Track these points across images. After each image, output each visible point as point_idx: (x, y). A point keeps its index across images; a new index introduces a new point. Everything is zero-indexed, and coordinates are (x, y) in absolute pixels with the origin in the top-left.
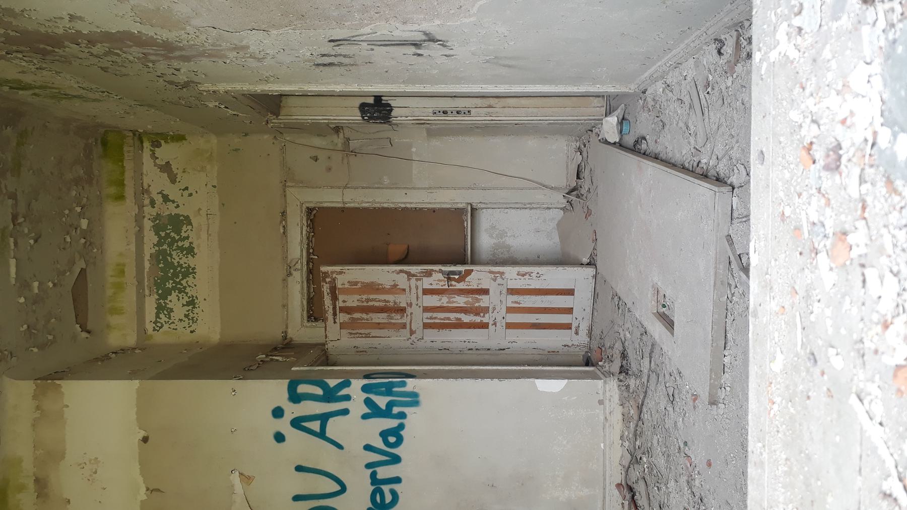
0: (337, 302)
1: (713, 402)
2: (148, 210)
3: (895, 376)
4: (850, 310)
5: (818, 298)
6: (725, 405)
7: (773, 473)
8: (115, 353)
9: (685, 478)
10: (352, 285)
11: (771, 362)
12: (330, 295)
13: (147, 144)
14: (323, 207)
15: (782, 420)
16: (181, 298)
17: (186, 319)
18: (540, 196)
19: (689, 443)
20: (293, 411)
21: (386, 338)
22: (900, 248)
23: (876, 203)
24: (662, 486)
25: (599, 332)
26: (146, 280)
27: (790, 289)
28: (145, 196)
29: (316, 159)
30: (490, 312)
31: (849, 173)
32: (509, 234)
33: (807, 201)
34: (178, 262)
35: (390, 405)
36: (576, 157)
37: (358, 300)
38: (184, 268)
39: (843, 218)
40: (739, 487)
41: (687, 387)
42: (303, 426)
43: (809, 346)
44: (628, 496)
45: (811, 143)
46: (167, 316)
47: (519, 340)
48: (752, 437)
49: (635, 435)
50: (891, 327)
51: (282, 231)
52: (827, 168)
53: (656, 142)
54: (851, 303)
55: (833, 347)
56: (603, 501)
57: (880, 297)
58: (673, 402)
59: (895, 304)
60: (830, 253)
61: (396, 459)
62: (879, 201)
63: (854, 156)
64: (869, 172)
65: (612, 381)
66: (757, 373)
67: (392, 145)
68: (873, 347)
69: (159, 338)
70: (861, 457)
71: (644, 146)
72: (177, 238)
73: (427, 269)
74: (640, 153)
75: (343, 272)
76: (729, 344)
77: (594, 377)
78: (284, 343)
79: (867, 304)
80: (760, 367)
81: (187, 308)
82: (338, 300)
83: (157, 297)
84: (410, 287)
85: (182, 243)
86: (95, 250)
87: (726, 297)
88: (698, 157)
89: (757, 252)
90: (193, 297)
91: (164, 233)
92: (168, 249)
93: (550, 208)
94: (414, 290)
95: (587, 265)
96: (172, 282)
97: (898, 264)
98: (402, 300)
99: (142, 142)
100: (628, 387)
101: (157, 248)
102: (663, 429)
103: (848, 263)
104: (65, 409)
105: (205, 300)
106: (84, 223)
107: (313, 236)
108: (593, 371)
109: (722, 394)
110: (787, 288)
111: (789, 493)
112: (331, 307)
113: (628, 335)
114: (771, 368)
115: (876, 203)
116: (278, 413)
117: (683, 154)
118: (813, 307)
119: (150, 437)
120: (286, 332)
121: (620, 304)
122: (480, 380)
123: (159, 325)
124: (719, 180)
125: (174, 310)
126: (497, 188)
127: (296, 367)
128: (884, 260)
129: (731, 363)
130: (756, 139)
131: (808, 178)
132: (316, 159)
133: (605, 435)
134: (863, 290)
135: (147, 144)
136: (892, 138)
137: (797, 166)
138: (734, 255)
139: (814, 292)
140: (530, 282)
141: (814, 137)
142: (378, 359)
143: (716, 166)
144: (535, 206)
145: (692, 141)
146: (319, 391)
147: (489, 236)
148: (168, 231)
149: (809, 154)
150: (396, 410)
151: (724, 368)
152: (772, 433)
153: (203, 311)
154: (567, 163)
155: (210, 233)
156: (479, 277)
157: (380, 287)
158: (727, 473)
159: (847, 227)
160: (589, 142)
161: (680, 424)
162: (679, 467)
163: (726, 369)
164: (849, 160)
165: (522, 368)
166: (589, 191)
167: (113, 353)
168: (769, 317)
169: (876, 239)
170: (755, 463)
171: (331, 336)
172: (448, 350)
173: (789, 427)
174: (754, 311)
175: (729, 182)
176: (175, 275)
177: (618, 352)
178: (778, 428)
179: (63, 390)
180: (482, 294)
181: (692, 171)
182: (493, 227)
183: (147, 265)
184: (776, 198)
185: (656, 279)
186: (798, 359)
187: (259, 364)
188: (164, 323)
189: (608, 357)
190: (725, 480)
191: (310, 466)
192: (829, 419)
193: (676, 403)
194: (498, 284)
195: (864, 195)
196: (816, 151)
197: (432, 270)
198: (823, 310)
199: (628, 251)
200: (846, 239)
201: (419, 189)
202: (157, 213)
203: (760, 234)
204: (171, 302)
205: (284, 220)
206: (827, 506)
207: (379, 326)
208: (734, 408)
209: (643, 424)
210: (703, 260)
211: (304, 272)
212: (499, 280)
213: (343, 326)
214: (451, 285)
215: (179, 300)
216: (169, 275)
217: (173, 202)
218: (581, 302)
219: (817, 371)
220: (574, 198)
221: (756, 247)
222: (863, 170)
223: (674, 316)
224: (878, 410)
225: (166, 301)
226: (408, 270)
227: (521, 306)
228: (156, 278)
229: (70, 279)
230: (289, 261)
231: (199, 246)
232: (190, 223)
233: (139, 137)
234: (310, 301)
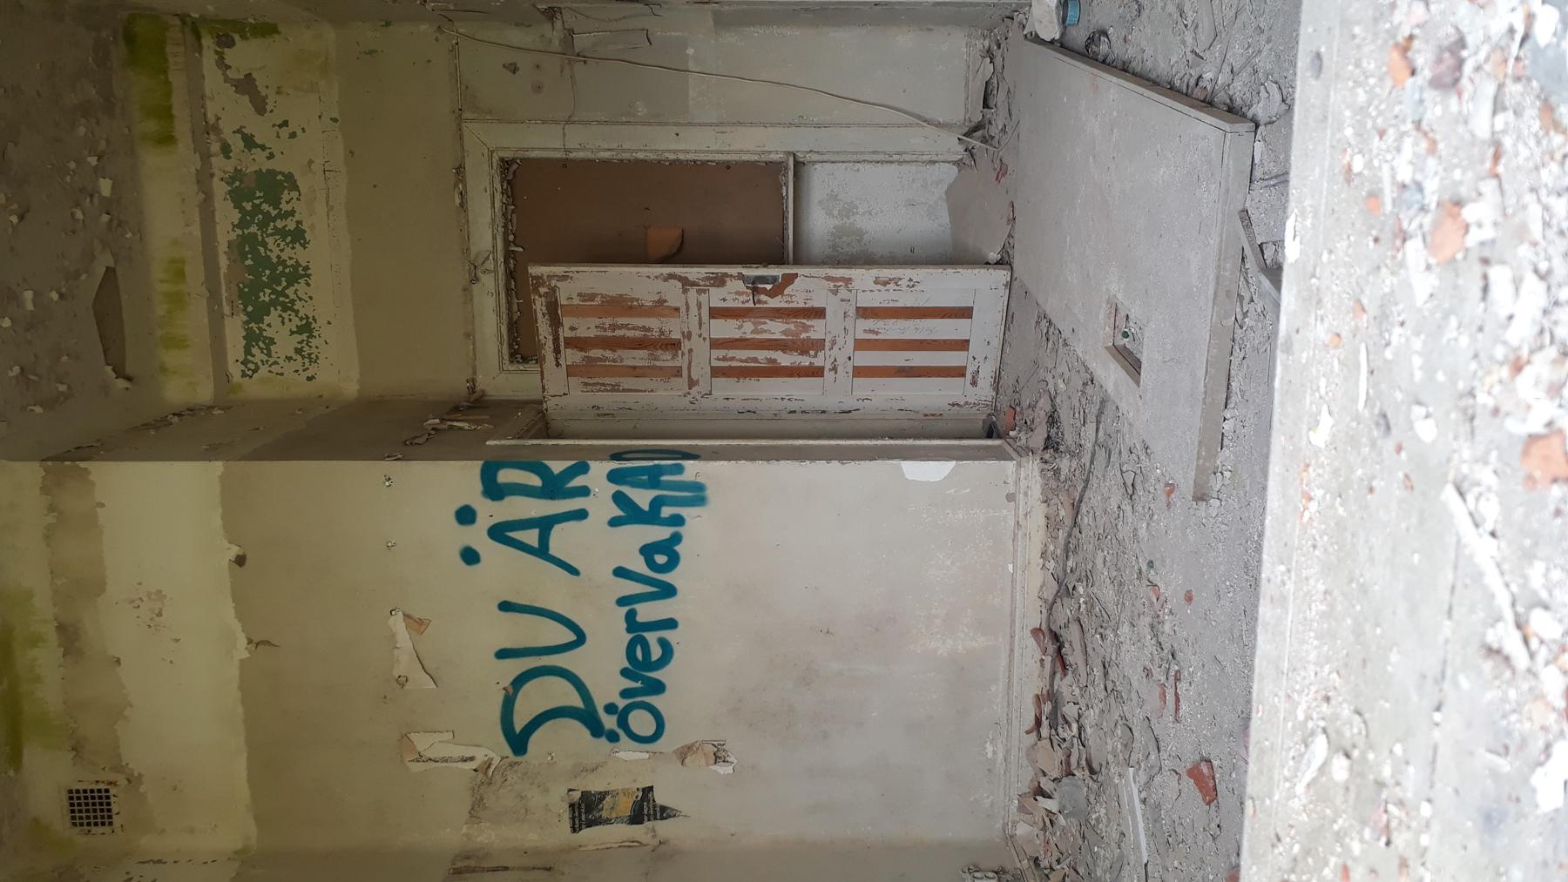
0: (561, 330)
1: (1201, 497)
2: (218, 162)
3: (1526, 453)
4: (1456, 339)
5: (1401, 319)
6: (1221, 501)
7: (1301, 616)
8: (179, 415)
9: (1148, 620)
10: (585, 301)
11: (1310, 429)
12: (547, 317)
13: (208, 42)
14: (529, 159)
15: (1323, 527)
16: (286, 321)
17: (299, 357)
18: (919, 140)
19: (1156, 564)
20: (490, 512)
21: (647, 393)
22: (1555, 229)
23: (1521, 147)
24: (1108, 632)
25: (1012, 381)
26: (224, 288)
27: (1351, 303)
28: (213, 137)
29: (514, 69)
30: (827, 348)
31: (1475, 92)
32: (861, 210)
33: (1396, 144)
34: (279, 257)
35: (657, 504)
36: (981, 69)
37: (596, 327)
38: (289, 267)
39: (1457, 174)
40: (1236, 634)
41: (1158, 470)
42: (509, 537)
43: (1378, 403)
44: (1051, 648)
45: (1411, 38)
46: (265, 351)
47: (875, 395)
48: (1269, 555)
49: (1067, 550)
50: (1527, 370)
51: (458, 201)
52: (1436, 83)
53: (1126, 41)
54: (1459, 327)
55: (1419, 403)
56: (1009, 656)
57: (1511, 317)
58: (1133, 497)
59: (1537, 329)
60: (1429, 239)
61: (668, 591)
62: (1526, 144)
63: (1487, 59)
64: (1513, 89)
65: (1031, 462)
66: (1284, 448)
67: (650, 43)
68: (1491, 403)
69: (254, 389)
70: (1453, 588)
71: (1103, 48)
72: (274, 213)
73: (717, 273)
74: (1097, 60)
75: (568, 276)
76: (1233, 399)
77: (1000, 455)
78: (472, 400)
79: (1486, 329)
80: (1291, 438)
81: (299, 338)
82: (562, 326)
83: (245, 318)
84: (687, 304)
85: (284, 223)
86: (129, 235)
87: (1233, 319)
88: (1197, 69)
89: (1298, 238)
90: (307, 317)
91: (251, 203)
92: (259, 233)
93: (934, 162)
94: (694, 310)
95: (995, 264)
96: (270, 291)
97: (1549, 259)
98: (674, 328)
99: (198, 37)
100: (1057, 472)
101: (239, 232)
102: (1114, 541)
103: (1459, 256)
104: (98, 510)
105: (329, 323)
106: (105, 187)
107: (513, 212)
108: (1000, 446)
109: (1216, 483)
110: (1347, 301)
111: (1326, 648)
112: (551, 338)
113: (1062, 386)
114: (1311, 440)
115: (1521, 147)
116: (466, 516)
117: (1171, 64)
118: (1390, 335)
119: (248, 557)
120: (473, 380)
121: (1050, 333)
122: (808, 462)
123: (252, 366)
124: (1233, 111)
125: (275, 341)
126: (840, 125)
127: (495, 439)
128: (1524, 251)
129: (1235, 432)
130: (1310, 30)
131: (1400, 103)
132: (514, 69)
133: (1015, 551)
134: (1482, 305)
135: (208, 42)
136: (1560, 27)
137: (1381, 79)
138: (1251, 246)
139: (1394, 309)
140: (892, 295)
141: (1418, 26)
142: (635, 427)
143: (1229, 85)
144: (907, 158)
145: (1189, 39)
146: (535, 481)
147: (826, 213)
148: (257, 202)
149: (1406, 58)
150: (666, 512)
151: (1222, 439)
152: (1305, 549)
153: (326, 343)
154: (967, 79)
155: (330, 203)
156: (808, 286)
157: (636, 303)
158: (1218, 612)
159: (1463, 191)
160: (1006, 39)
161: (1142, 533)
162: (1138, 603)
163: (1226, 442)
164: (1478, 69)
165: (880, 442)
166: (1004, 130)
167: (174, 414)
168: (1311, 353)
169: (1514, 214)
170: (1272, 598)
171: (551, 390)
172: (754, 412)
173: (1333, 540)
174: (1286, 342)
175: (1250, 114)
176: (275, 279)
177: (1042, 413)
178: (1315, 540)
179: (92, 477)
180: (813, 316)
181: (1186, 95)
182: (834, 197)
183: (223, 262)
184: (1339, 141)
185: (1115, 287)
186: (1359, 423)
187: (429, 434)
188: (260, 363)
189: (1026, 423)
190: (1214, 623)
191: (524, 603)
192: (1403, 526)
193: (1138, 498)
194: (842, 300)
195: (1499, 133)
196: (1419, 51)
197: (726, 275)
198: (1407, 340)
199: (1068, 239)
200: (1459, 214)
202: (236, 169)
203: (1305, 204)
204: (270, 327)
205: (461, 181)
206: (1389, 668)
207: (635, 371)
208: (1236, 506)
209: (1080, 532)
210: (1197, 253)
211: (500, 275)
212: (843, 293)
213: (572, 371)
214: (760, 302)
215: (283, 323)
216: (264, 279)
217: (263, 148)
218: (984, 330)
219: (1389, 445)
220: (977, 144)
221: (1297, 229)
222: (1501, 86)
223: (1142, 353)
224: (1491, 511)
225: (261, 325)
226: (683, 275)
227: (879, 337)
228: (241, 285)
229: (90, 284)
230: (472, 256)
231: (312, 227)
232: (294, 187)
233: (194, 28)
234: (513, 326)
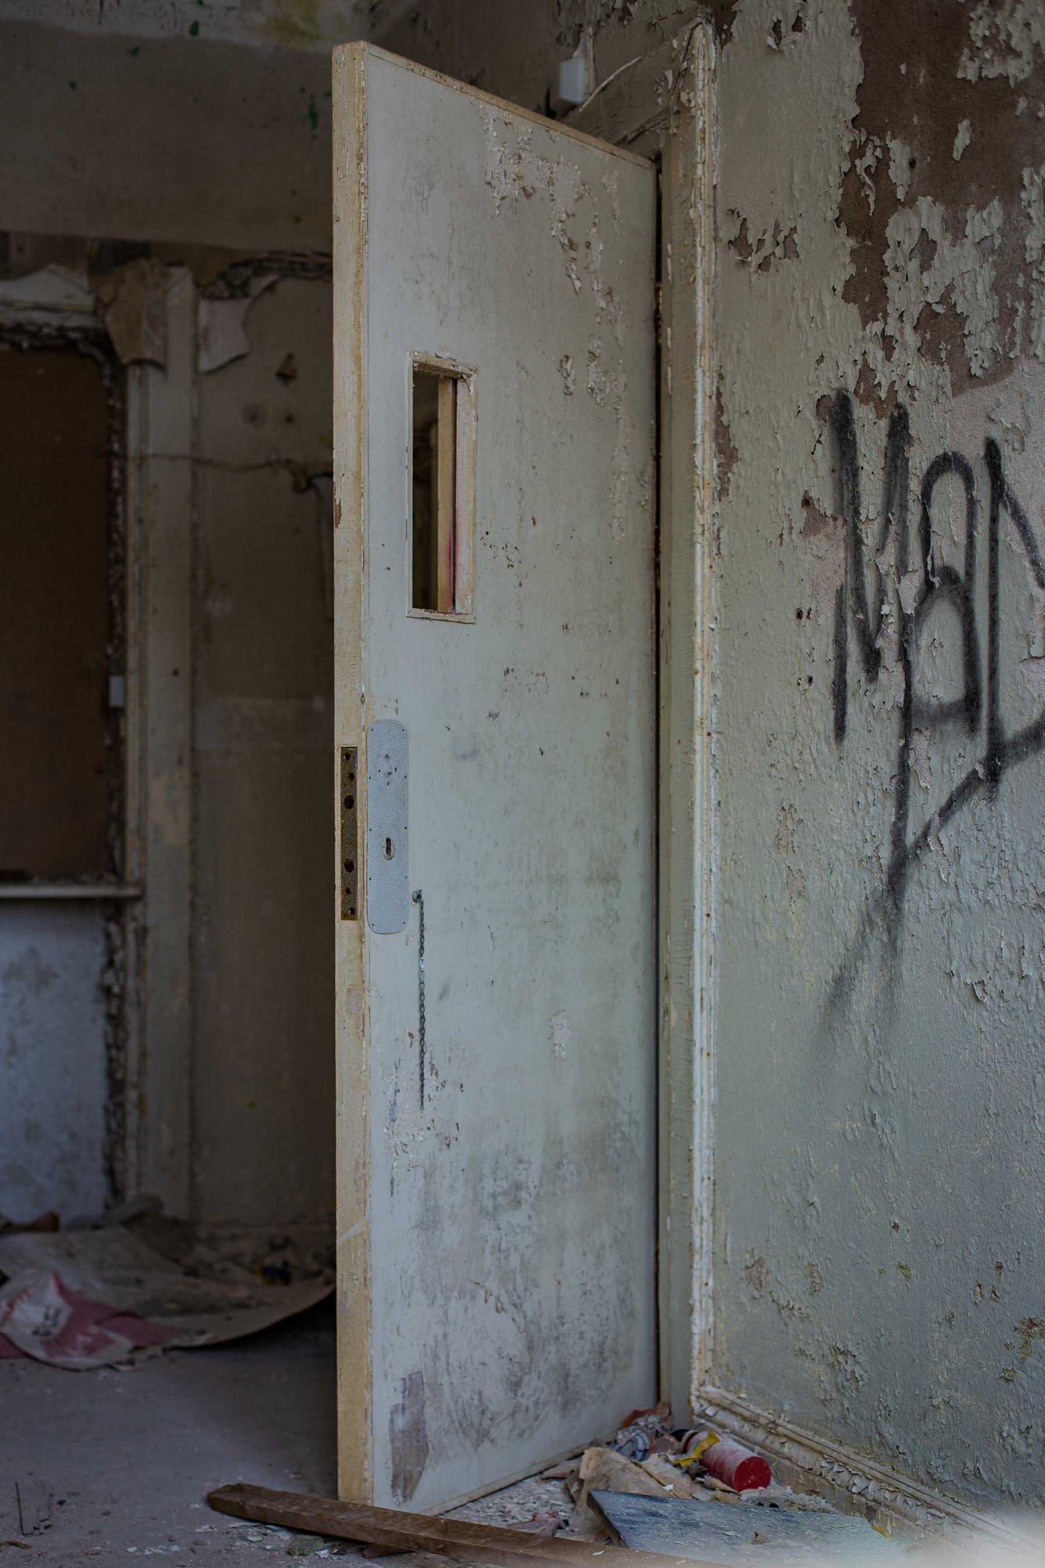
201: (193, 717)
